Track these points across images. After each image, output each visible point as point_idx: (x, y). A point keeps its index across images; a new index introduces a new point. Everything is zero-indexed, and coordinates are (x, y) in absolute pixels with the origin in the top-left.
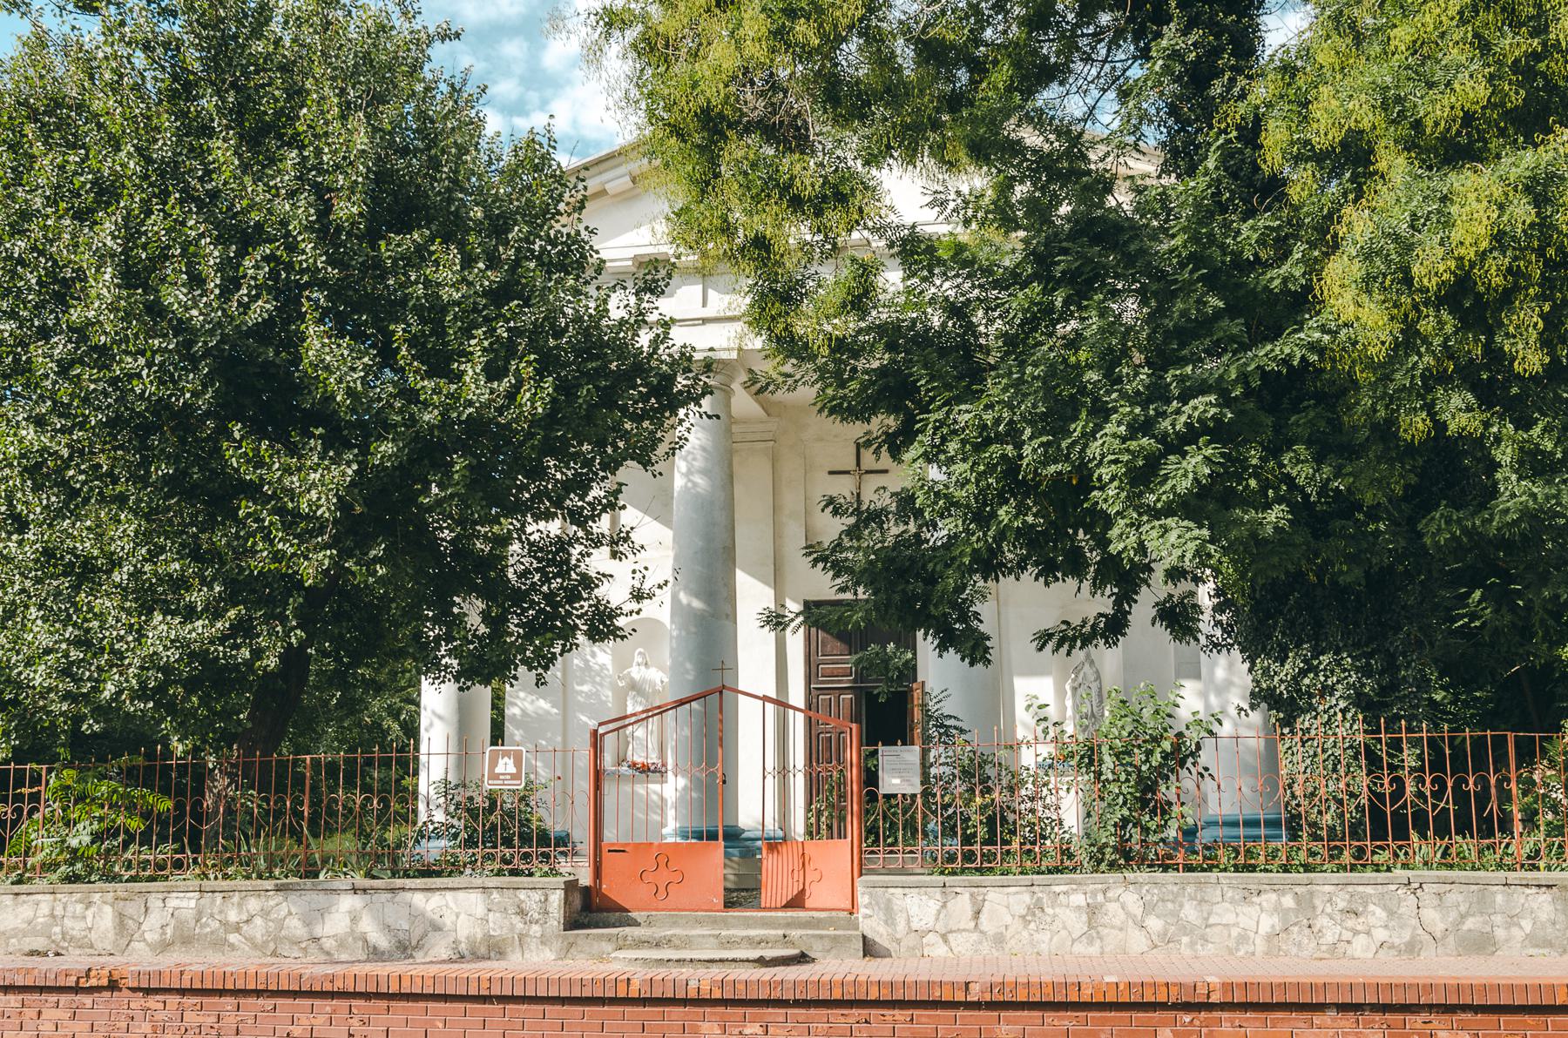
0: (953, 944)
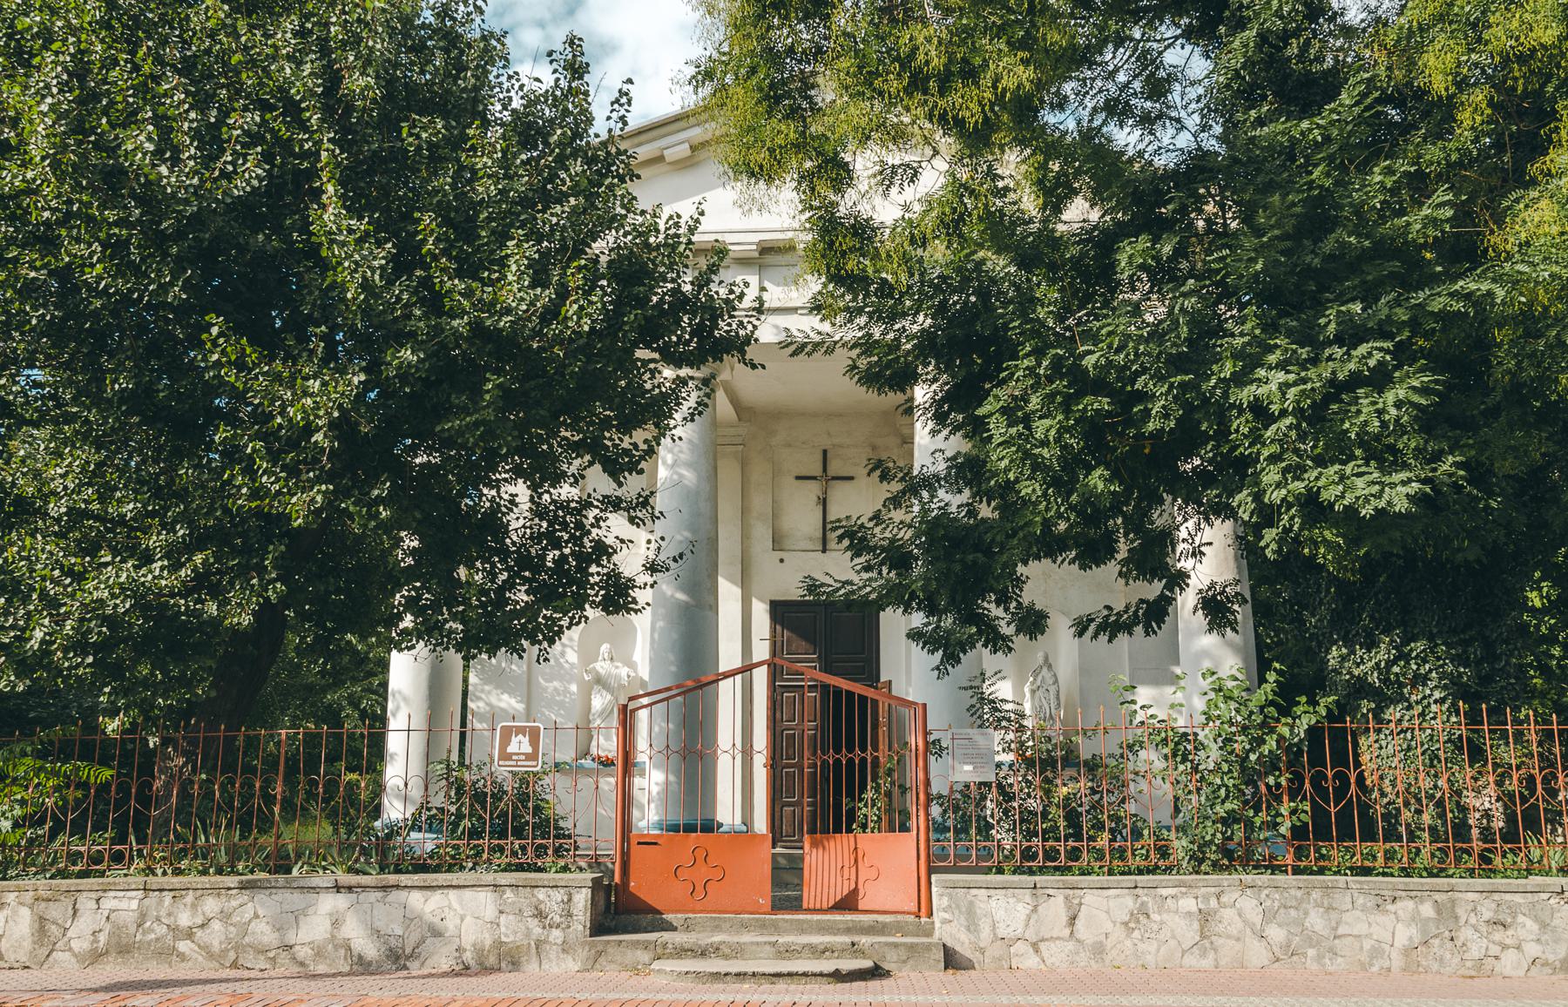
0: (1045, 954)
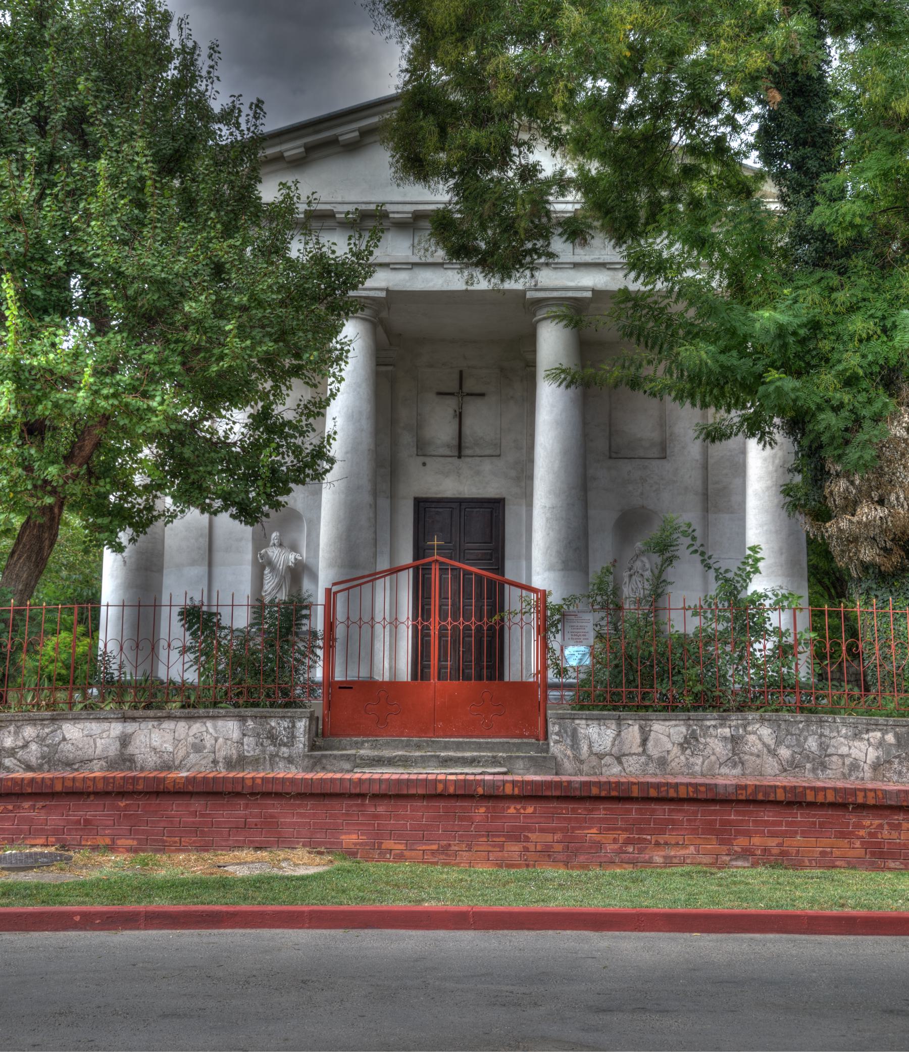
0: (626, 765)
